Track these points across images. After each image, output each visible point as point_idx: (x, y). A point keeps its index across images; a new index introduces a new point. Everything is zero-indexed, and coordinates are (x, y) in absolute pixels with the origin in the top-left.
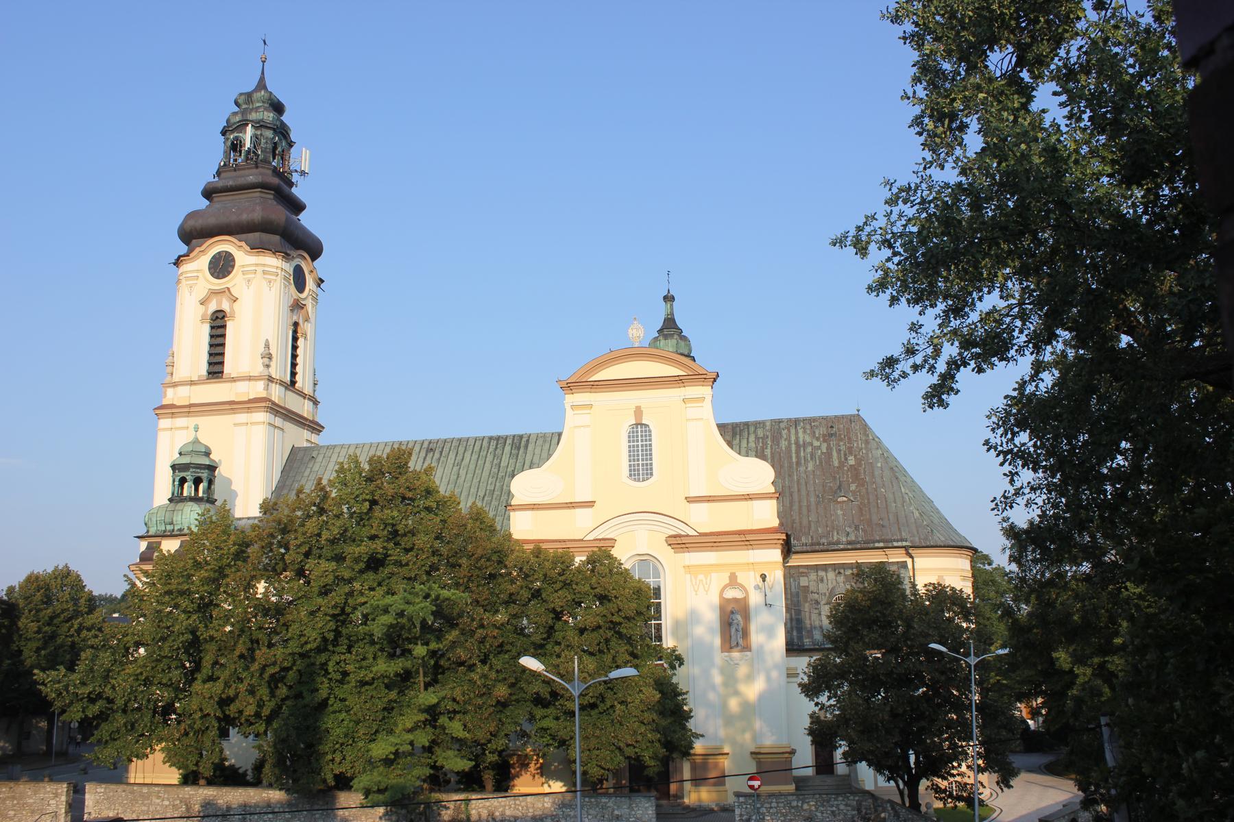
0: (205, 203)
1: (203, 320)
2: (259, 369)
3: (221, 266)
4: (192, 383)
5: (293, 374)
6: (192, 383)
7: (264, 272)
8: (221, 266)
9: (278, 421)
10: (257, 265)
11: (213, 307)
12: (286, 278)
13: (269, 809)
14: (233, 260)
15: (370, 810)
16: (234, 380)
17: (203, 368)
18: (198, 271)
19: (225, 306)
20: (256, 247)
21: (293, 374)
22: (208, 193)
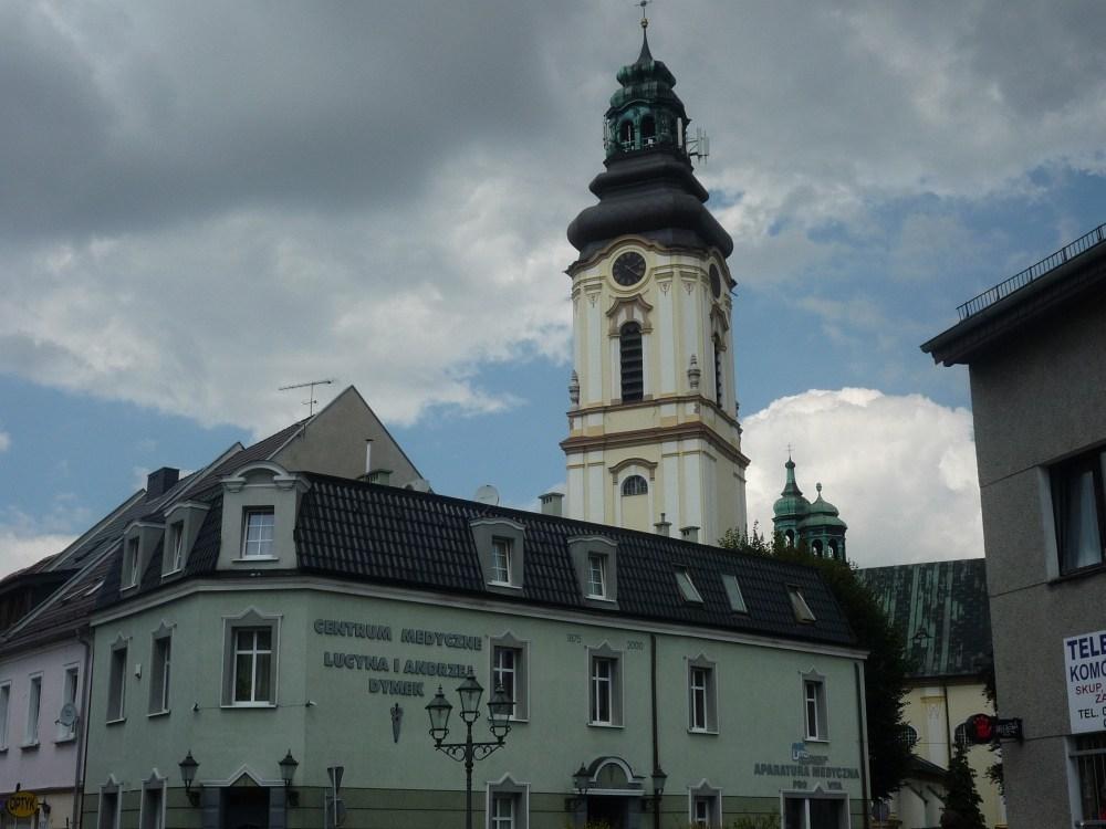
0: (594, 201)
1: (612, 336)
2: (685, 389)
3: (629, 271)
4: (605, 410)
5: (719, 395)
6: (605, 410)
7: (587, 288)
8: (629, 271)
9: (712, 451)
10: (672, 266)
11: (622, 318)
12: (704, 279)
13: (1042, 566)
14: (643, 262)
15: (1005, 777)
16: (657, 403)
17: (615, 392)
18: (600, 278)
19: (638, 316)
20: (672, 248)
21: (719, 395)
22: (599, 187)
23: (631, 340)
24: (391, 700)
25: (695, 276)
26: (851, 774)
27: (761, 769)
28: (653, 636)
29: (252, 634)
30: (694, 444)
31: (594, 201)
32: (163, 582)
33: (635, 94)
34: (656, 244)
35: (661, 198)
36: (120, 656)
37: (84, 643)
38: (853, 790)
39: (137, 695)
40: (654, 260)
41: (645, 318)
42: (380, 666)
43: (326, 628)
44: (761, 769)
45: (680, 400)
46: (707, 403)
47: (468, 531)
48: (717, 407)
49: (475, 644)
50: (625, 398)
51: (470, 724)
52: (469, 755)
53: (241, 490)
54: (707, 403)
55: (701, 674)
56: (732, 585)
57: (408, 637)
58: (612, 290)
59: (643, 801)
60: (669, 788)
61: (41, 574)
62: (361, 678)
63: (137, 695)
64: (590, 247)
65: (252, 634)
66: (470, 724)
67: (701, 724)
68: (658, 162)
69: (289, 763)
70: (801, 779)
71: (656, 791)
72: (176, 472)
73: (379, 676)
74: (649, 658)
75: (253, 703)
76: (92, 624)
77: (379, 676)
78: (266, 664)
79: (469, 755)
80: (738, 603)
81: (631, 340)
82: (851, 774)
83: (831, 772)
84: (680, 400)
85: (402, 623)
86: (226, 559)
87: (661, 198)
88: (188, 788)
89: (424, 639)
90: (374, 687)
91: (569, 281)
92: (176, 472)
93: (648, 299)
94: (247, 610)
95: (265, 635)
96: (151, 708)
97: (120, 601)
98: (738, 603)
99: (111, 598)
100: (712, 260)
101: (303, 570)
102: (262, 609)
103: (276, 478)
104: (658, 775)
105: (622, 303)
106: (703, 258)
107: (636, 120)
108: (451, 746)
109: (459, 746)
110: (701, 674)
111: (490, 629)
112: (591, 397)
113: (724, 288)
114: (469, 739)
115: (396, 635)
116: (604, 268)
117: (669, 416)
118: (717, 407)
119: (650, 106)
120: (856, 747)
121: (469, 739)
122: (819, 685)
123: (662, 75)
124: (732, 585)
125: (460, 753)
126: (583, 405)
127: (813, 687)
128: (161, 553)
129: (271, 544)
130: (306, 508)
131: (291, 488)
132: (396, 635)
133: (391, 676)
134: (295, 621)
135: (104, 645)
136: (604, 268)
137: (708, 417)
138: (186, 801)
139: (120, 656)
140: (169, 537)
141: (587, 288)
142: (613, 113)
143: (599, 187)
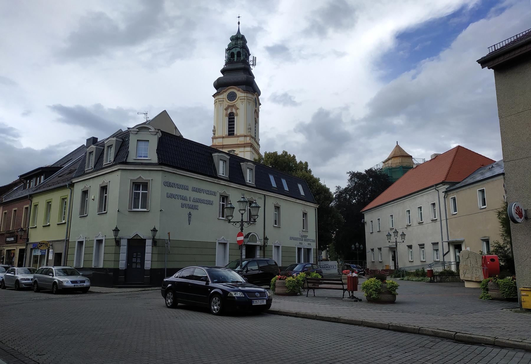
1: (226, 115)
3: (232, 97)
8: (232, 97)
11: (229, 111)
16: (238, 137)
17: (226, 132)
19: (234, 111)
23: (231, 118)
24: (188, 211)
25: (251, 100)
26: (313, 241)
27: (292, 238)
28: (265, 195)
29: (140, 186)
30: (248, 149)
31: (221, 75)
32: (103, 166)
33: (235, 44)
34: (240, 89)
35: (241, 76)
36: (85, 193)
37: (70, 189)
38: (313, 246)
39: (93, 205)
40: (240, 94)
41: (236, 111)
42: (184, 198)
43: (167, 184)
44: (292, 238)
45: (245, 136)
46: (253, 138)
47: (212, 157)
48: (255, 139)
49: (214, 194)
50: (229, 134)
51: (242, 214)
52: (242, 226)
53: (136, 134)
54: (253, 138)
55: (277, 208)
56: (274, 184)
57: (195, 190)
58: (227, 103)
59: (261, 247)
60: (269, 243)
61: (55, 167)
62: (179, 202)
63: (93, 205)
64: (220, 89)
65: (140, 186)
66: (242, 214)
67: (276, 224)
68: (241, 66)
69: (154, 230)
70: (301, 242)
71: (264, 243)
72: (97, 139)
73: (184, 202)
74: (263, 202)
75: (140, 209)
76: (73, 182)
77: (184, 202)
78: (145, 196)
79: (242, 226)
80: (286, 188)
81: (231, 118)
82: (313, 241)
83: (308, 240)
84: (245, 136)
85: (192, 183)
86: (131, 158)
87: (241, 76)
88: (115, 239)
89: (199, 191)
90: (183, 206)
91: (213, 99)
92: (97, 139)
93: (237, 106)
94: (138, 177)
95: (145, 186)
96: (99, 211)
97: (85, 174)
98: (286, 188)
99: (82, 172)
100: (255, 96)
101: (160, 164)
102: (145, 177)
103: (150, 130)
104: (266, 239)
105: (229, 106)
106: (253, 95)
107: (235, 52)
108: (234, 222)
109: (238, 222)
110: (277, 208)
111: (219, 190)
112: (219, 134)
113: (258, 104)
114: (242, 220)
115: (190, 189)
116: (225, 95)
117: (241, 140)
118: (255, 139)
119: (240, 48)
120: (315, 233)
121: (242, 220)
122: (306, 214)
123: (243, 38)
124: (274, 184)
125: (238, 225)
126: (216, 136)
127: (305, 215)
128: (103, 157)
129: (150, 152)
130: (161, 142)
131: (155, 135)
132: (190, 189)
133: (188, 202)
134: (157, 180)
135: (78, 189)
136: (225, 95)
137: (253, 141)
138: (114, 243)
139: (85, 193)
140: (109, 152)
141: (219, 101)
142: (228, 50)
143: (223, 71)
